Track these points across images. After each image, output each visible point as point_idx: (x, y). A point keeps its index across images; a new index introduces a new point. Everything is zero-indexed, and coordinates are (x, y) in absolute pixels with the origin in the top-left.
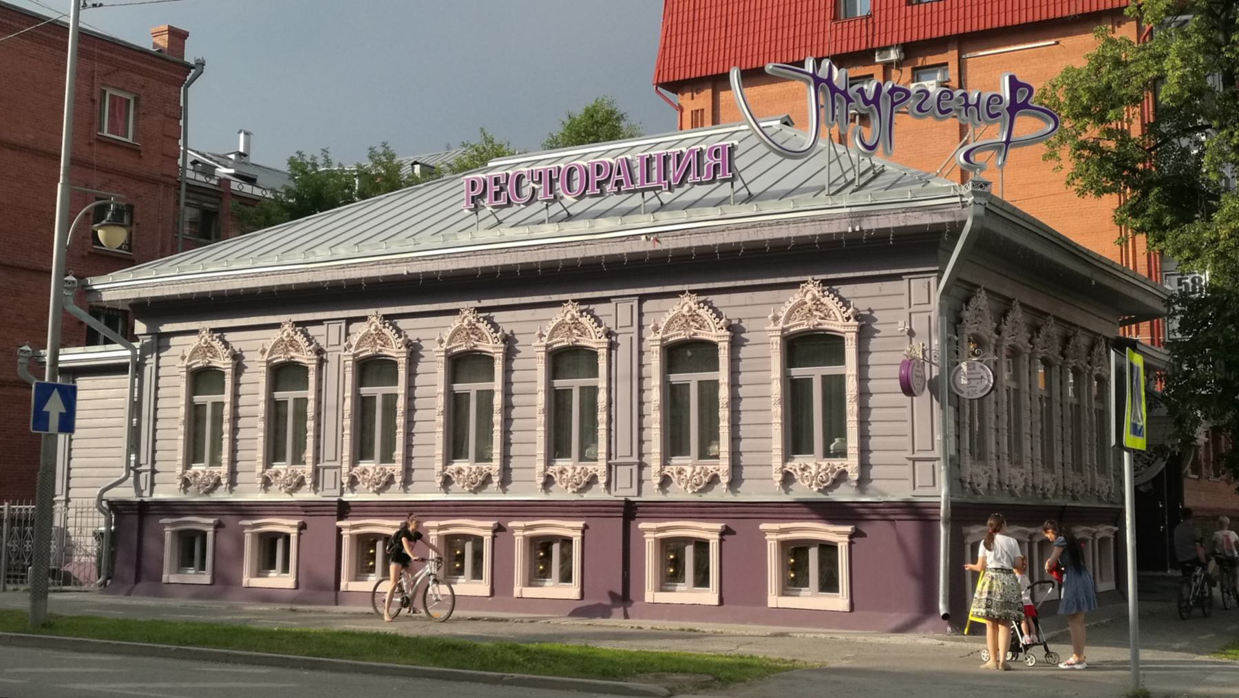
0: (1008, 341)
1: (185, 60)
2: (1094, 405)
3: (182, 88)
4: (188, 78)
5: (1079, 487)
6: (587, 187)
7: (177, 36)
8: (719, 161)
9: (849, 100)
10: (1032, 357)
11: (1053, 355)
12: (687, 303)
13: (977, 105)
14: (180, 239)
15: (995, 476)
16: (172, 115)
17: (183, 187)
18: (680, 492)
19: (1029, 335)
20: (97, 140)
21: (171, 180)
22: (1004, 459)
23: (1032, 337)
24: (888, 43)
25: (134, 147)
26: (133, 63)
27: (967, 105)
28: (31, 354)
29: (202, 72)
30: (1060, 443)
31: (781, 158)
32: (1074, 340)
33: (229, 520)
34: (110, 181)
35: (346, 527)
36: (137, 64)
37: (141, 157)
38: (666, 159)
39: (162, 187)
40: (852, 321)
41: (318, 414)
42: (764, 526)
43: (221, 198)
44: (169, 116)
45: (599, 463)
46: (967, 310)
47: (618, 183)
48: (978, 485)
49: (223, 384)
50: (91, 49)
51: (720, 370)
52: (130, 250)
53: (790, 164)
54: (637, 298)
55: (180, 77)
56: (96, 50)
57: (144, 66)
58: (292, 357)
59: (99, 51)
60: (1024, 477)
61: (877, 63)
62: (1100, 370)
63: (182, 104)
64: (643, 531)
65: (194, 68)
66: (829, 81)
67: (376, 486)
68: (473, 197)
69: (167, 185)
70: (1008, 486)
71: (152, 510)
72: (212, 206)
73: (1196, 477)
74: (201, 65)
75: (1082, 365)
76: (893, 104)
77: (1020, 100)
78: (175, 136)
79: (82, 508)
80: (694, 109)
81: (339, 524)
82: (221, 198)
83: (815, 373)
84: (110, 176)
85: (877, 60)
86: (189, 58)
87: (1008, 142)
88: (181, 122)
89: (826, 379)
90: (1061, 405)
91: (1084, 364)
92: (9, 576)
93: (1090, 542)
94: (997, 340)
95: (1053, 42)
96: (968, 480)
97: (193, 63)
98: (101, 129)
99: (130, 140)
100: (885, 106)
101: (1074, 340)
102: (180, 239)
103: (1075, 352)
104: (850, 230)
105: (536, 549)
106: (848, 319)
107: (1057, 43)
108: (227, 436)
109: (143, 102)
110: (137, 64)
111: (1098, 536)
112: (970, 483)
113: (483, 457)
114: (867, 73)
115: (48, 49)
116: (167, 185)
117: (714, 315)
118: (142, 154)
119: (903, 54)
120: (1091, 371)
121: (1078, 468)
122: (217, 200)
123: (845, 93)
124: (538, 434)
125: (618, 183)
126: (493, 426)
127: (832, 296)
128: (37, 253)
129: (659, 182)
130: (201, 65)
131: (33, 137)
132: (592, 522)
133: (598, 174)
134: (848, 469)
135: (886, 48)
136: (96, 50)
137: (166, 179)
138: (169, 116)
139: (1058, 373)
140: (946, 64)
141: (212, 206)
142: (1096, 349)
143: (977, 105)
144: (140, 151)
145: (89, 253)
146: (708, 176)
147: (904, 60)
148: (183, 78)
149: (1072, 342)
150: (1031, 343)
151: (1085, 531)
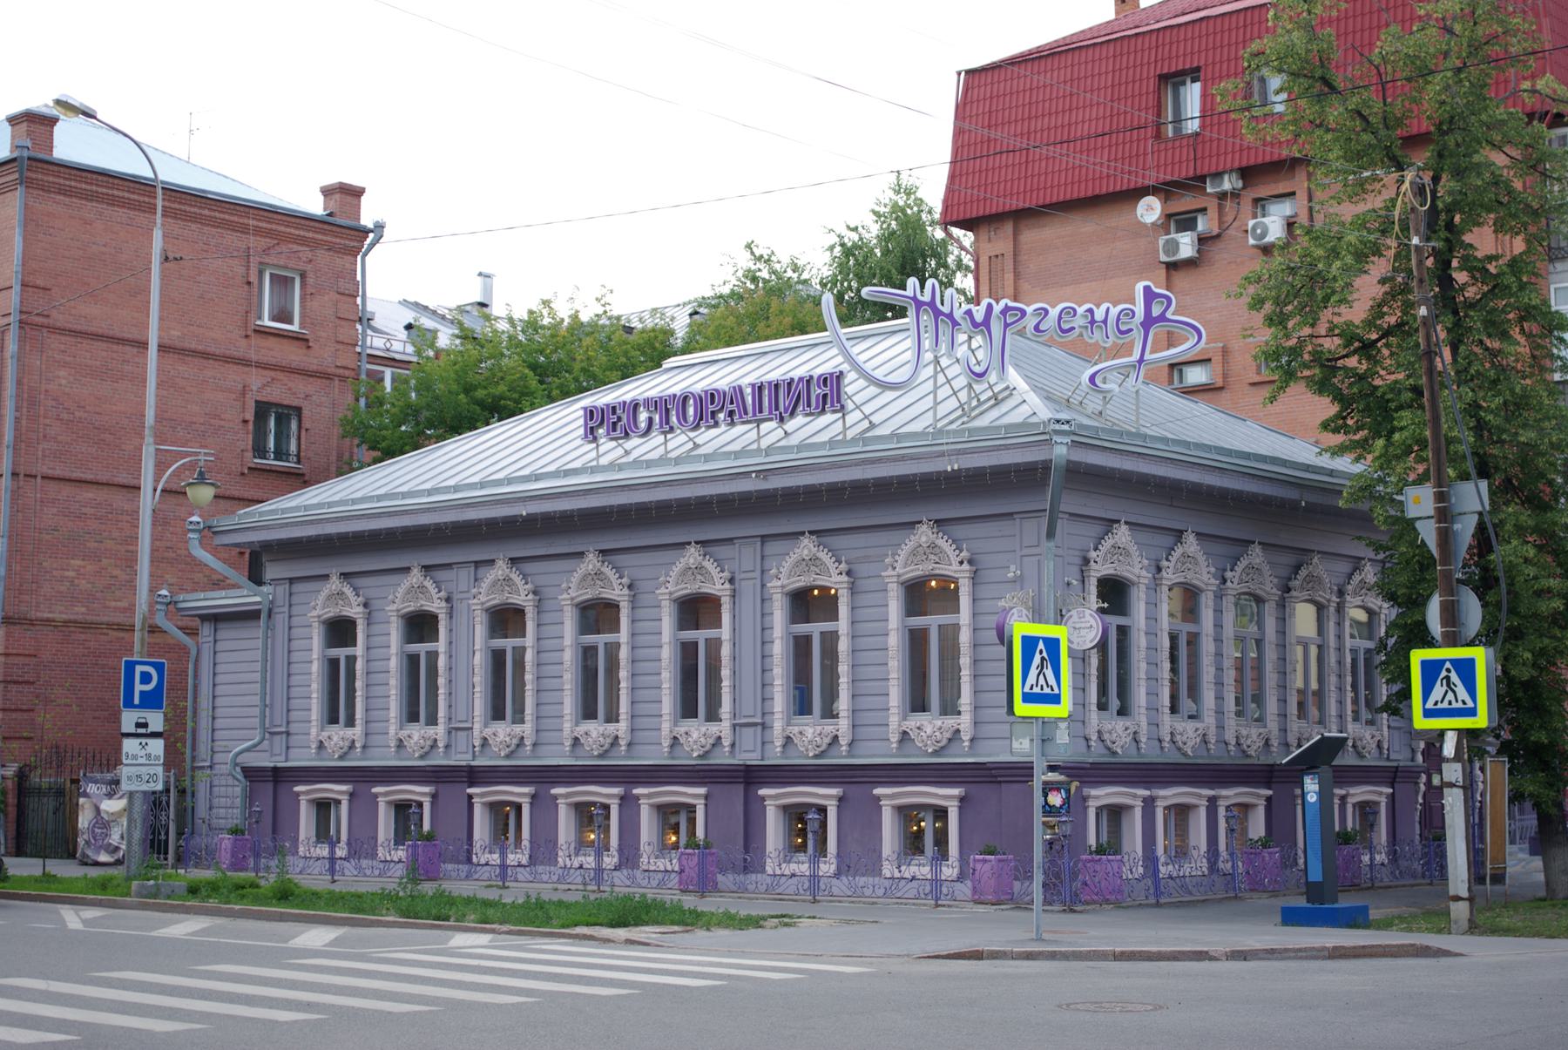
3: (359, 258)
6: (701, 419)
7: (346, 195)
8: (827, 390)
9: (955, 323)
10: (1219, 596)
12: (807, 547)
13: (1105, 321)
18: (804, 755)
20: (255, 331)
21: (347, 373)
24: (1221, 169)
26: (297, 232)
27: (1093, 322)
28: (169, 599)
31: (879, 390)
34: (273, 379)
35: (477, 795)
36: (302, 233)
37: (309, 347)
38: (777, 386)
39: (337, 382)
44: (343, 294)
45: (723, 724)
47: (731, 414)
49: (437, 630)
50: (246, 221)
52: (299, 462)
53: (890, 395)
55: (356, 244)
56: (251, 222)
57: (310, 235)
58: (1357, 460)
59: (255, 223)
61: (1210, 194)
63: (359, 278)
64: (763, 799)
66: (932, 304)
68: (592, 428)
69: (343, 379)
74: (379, 227)
76: (1006, 325)
77: (1156, 312)
80: (993, 254)
81: (470, 791)
84: (272, 374)
86: (367, 220)
87: (1141, 360)
97: (371, 226)
98: (260, 318)
99: (295, 327)
100: (996, 326)
104: (949, 469)
105: (790, 820)
106: (961, 563)
108: (667, 692)
109: (310, 280)
110: (302, 233)
113: (432, 720)
114: (1198, 207)
115: (194, 226)
116: (343, 379)
117: (954, 546)
123: (950, 316)
124: (664, 692)
125: (731, 414)
126: (437, 689)
127: (946, 537)
129: (770, 413)
130: (379, 227)
132: (717, 789)
133: (712, 403)
134: (961, 727)
135: (1218, 175)
136: (251, 222)
137: (341, 371)
138: (343, 294)
140: (1293, 194)
143: (1105, 321)
144: (307, 340)
145: (250, 468)
146: (817, 407)
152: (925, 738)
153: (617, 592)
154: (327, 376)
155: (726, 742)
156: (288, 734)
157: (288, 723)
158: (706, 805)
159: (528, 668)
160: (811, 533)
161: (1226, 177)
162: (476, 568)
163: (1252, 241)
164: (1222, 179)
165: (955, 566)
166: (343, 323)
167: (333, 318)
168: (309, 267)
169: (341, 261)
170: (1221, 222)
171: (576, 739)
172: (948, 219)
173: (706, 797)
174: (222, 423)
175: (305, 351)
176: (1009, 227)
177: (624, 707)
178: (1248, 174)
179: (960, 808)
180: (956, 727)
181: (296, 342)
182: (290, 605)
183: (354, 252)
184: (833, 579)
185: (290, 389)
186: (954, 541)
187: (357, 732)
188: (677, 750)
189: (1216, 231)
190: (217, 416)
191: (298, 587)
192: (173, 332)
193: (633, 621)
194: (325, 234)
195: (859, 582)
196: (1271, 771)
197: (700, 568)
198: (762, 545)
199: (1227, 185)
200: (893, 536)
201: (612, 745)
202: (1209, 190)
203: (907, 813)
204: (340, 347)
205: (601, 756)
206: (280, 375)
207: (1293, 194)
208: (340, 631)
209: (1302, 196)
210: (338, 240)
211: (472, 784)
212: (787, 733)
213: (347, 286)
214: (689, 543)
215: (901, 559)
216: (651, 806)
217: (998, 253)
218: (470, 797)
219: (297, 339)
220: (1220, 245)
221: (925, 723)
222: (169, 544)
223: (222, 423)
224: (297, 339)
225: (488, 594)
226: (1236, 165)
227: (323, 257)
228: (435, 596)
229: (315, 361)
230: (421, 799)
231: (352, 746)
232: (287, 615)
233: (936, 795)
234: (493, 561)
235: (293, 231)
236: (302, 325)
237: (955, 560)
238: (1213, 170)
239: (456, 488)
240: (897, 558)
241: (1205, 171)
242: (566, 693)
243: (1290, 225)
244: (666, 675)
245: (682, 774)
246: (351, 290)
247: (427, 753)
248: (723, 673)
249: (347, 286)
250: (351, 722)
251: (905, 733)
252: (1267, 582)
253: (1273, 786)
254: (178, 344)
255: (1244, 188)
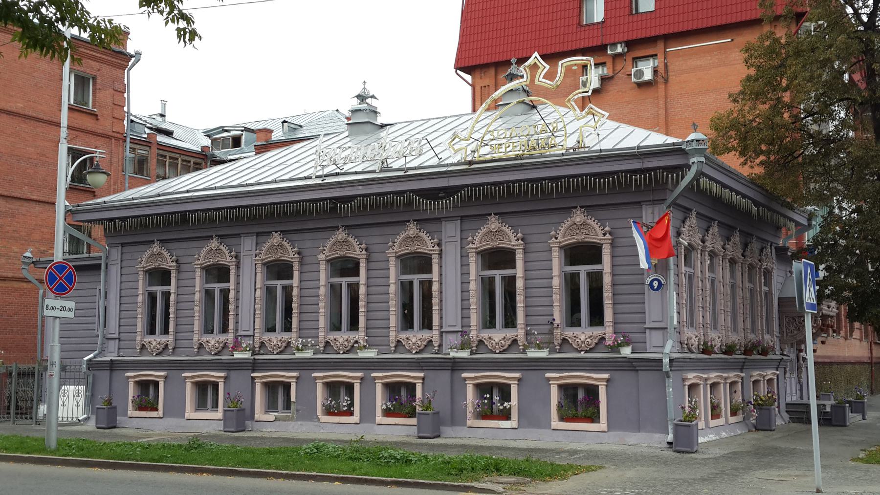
0: (730, 254)
1: (128, 51)
2: (707, 274)
3: (126, 71)
4: (130, 64)
5: (716, 341)
11: (694, 241)
14: (127, 177)
15: (702, 338)
16: (119, 90)
17: (128, 140)
19: (722, 243)
21: (119, 136)
22: (684, 326)
23: (725, 244)
24: (616, 41)
25: (93, 112)
26: (91, 53)
29: (140, 60)
30: (742, 315)
31: (471, 82)
32: (751, 245)
33: (532, 376)
36: (94, 54)
37: (97, 119)
40: (608, 236)
41: (237, 299)
42: (315, 375)
43: (150, 147)
46: (684, 227)
48: (692, 345)
51: (517, 268)
54: (460, 218)
55: (124, 63)
60: (720, 339)
61: (609, 55)
62: (767, 265)
63: (126, 82)
65: (134, 57)
67: (279, 350)
69: (117, 139)
70: (686, 344)
71: (257, 367)
72: (144, 152)
73: (826, 335)
74: (138, 54)
75: (755, 262)
78: (121, 104)
79: (76, 366)
82: (150, 147)
83: (583, 270)
84: (77, 133)
85: (609, 52)
86: (130, 49)
88: (126, 95)
89: (589, 274)
90: (742, 289)
91: (757, 261)
92: (17, 414)
93: (740, 383)
94: (702, 247)
95: (730, 40)
96: (686, 342)
97: (133, 53)
101: (751, 245)
102: (127, 177)
103: (751, 253)
106: (604, 235)
107: (732, 40)
109: (99, 81)
110: (94, 54)
111: (767, 378)
112: (686, 344)
116: (117, 139)
118: (99, 117)
119: (626, 48)
120: (761, 266)
121: (753, 331)
122: (148, 148)
127: (593, 219)
128: (26, 187)
130: (138, 54)
131: (22, 105)
135: (614, 45)
137: (115, 135)
139: (740, 268)
140: (656, 55)
141: (144, 152)
142: (764, 251)
144: (97, 115)
147: (627, 52)
148: (127, 64)
149: (749, 247)
150: (723, 248)
151: (772, 373)
152: (210, 347)
153: (358, 253)
154: (108, 137)
155: (436, 344)
156: (119, 339)
157: (119, 333)
158: (423, 383)
159: (294, 299)
160: (414, 221)
161: (619, 46)
162: (257, 236)
163: (634, 80)
164: (617, 47)
165: (514, 242)
166: (117, 107)
167: (111, 104)
168: (98, 74)
169: (116, 72)
170: (614, 70)
171: (262, 343)
172: (459, 66)
173: (225, 378)
174: (47, 159)
175: (95, 121)
176: (492, 71)
177: (295, 324)
178: (630, 44)
179: (165, 381)
180: (602, 335)
181: (90, 116)
182: (122, 261)
183: (123, 67)
184: (512, 243)
185: (87, 142)
186: (227, 246)
187: (170, 338)
188: (202, 350)
189: (611, 74)
190: (44, 155)
191: (126, 249)
192: (19, 105)
193: (368, 270)
194: (106, 55)
195: (617, 240)
196: (744, 363)
197: (417, 237)
198: (461, 222)
199: (619, 49)
200: (554, 218)
201: (164, 349)
202: (608, 53)
203: (483, 389)
204: (115, 120)
205: (216, 354)
206: (82, 134)
207: (656, 55)
208: (219, 273)
209: (661, 56)
210: (114, 60)
211: (254, 371)
212: (480, 338)
213: (119, 86)
214: (490, 215)
215: (477, 239)
216: (262, 383)
217: (486, 85)
218: (253, 378)
219: (91, 114)
220: (613, 82)
221: (411, 336)
222: (15, 229)
223: (47, 159)
224: (91, 114)
225: (266, 254)
226: (625, 39)
227: (106, 69)
228: (290, 250)
229: (101, 127)
230: (158, 380)
231: (225, 346)
232: (119, 266)
233: (153, 376)
234: (271, 232)
235: (89, 52)
236: (94, 106)
237: (513, 239)
238: (612, 42)
239: (275, 182)
240: (143, 259)
241: (607, 42)
242: (321, 314)
243: (655, 71)
244: (392, 303)
245: (281, 365)
246: (121, 90)
247: (219, 352)
248: (433, 301)
249: (119, 86)
250: (166, 331)
251: (399, 341)
252: (429, 242)
253: (744, 370)
254: (21, 112)
255: (628, 52)
